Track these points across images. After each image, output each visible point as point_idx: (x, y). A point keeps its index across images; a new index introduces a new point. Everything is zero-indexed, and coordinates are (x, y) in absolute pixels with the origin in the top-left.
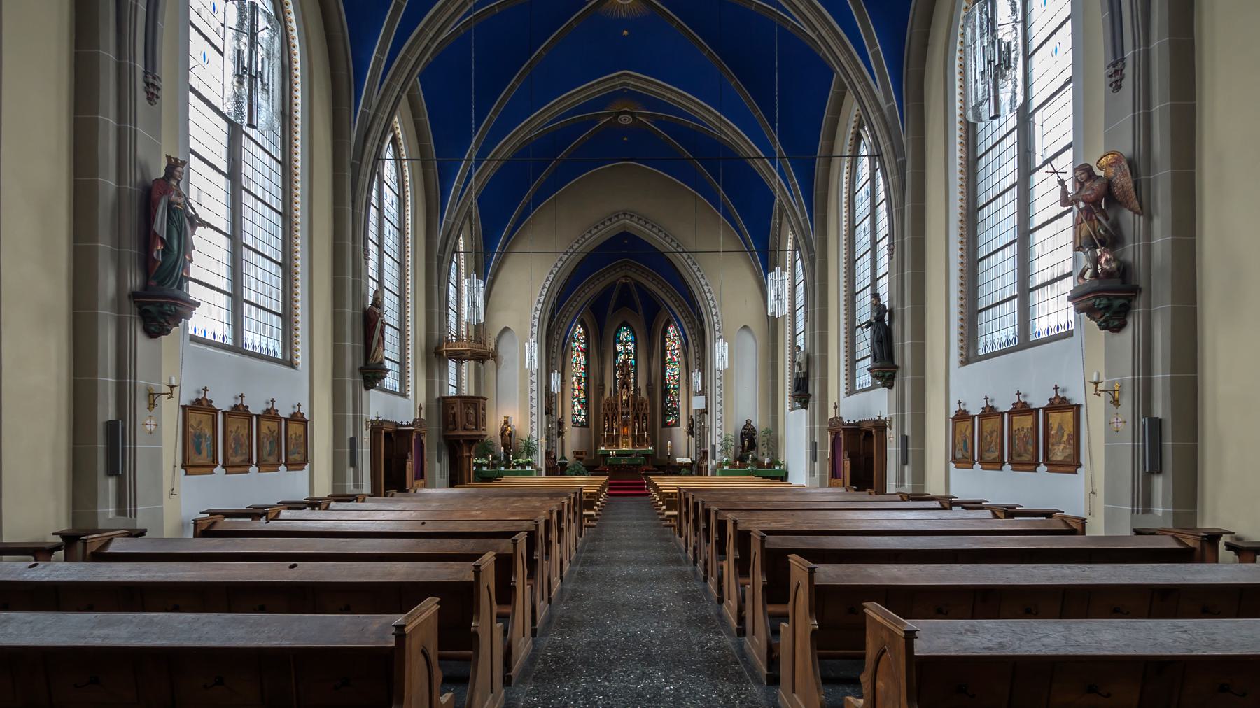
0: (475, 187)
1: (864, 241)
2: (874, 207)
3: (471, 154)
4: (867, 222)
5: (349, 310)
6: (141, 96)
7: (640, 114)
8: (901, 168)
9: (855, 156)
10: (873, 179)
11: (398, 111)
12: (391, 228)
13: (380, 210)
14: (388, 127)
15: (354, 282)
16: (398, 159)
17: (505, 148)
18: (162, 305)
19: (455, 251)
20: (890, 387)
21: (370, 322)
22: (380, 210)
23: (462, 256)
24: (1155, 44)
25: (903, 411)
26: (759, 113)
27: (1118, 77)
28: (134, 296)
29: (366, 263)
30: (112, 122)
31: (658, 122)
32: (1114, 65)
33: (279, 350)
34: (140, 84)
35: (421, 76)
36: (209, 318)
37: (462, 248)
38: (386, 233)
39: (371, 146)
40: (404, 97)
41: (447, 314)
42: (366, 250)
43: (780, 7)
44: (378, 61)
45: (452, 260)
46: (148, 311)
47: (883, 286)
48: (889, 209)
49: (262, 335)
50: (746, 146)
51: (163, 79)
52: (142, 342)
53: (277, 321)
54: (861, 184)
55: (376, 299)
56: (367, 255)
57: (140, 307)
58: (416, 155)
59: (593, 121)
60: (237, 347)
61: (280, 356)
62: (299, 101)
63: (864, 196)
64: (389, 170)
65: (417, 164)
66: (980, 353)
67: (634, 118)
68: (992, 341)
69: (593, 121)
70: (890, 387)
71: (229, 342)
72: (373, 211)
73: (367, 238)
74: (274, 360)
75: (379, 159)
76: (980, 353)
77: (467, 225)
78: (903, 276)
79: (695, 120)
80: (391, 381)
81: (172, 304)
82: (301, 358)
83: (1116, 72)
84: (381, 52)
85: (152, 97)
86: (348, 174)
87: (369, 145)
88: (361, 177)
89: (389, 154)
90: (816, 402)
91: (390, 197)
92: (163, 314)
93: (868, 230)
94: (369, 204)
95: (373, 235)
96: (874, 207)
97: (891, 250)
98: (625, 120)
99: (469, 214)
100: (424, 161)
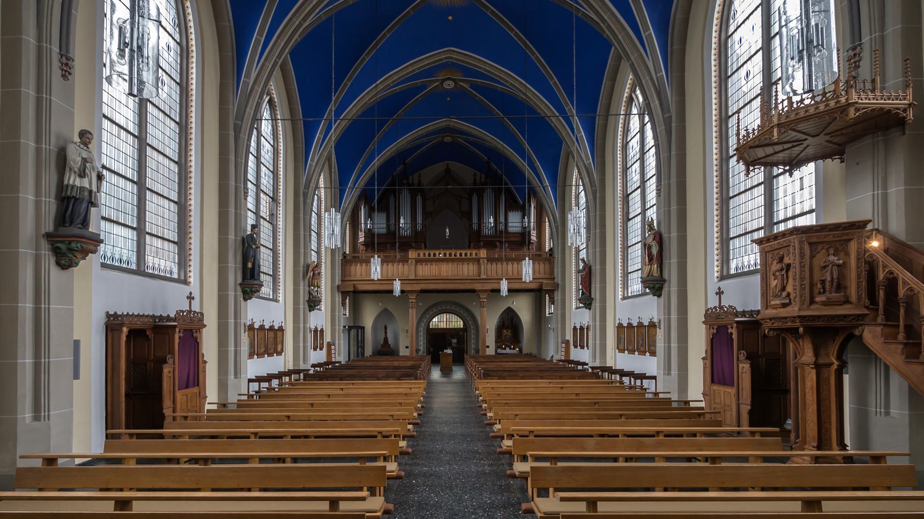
0: (333, 135)
1: (635, 179)
2: (643, 153)
3: (331, 110)
4: (637, 165)
5: (231, 237)
6: (57, 73)
7: (461, 80)
8: (668, 122)
9: (628, 114)
10: (642, 131)
11: (273, 78)
12: (267, 171)
13: (258, 158)
14: (265, 90)
15: (236, 213)
16: (274, 119)
17: (353, 110)
18: (70, 243)
19: (317, 187)
20: (659, 296)
21: (249, 247)
22: (258, 158)
23: (323, 191)
24: (889, 30)
25: (669, 314)
26: (554, 82)
27: (857, 58)
28: (48, 236)
29: (246, 199)
30: (32, 93)
31: (474, 86)
32: (854, 49)
33: (175, 270)
34: (56, 64)
35: (292, 53)
36: (117, 242)
37: (322, 184)
38: (263, 175)
39: (250, 111)
40: (277, 68)
41: (310, 235)
42: (246, 188)
43: (577, 3)
44: (258, 41)
45: (314, 194)
46: (60, 248)
47: (652, 214)
48: (658, 154)
49: (162, 258)
50: (544, 106)
51: (76, 60)
52: (55, 273)
53: (174, 248)
54: (633, 134)
55: (253, 227)
56: (246, 193)
57: (52, 245)
58: (288, 116)
59: (424, 87)
60: (140, 271)
61: (175, 276)
62: (194, 76)
63: (635, 146)
64: (266, 127)
65: (288, 123)
66: (732, 272)
67: (456, 83)
68: (743, 263)
69: (424, 87)
70: (659, 296)
71: (134, 267)
72: (251, 158)
73: (246, 180)
74: (171, 280)
75: (257, 119)
76: (732, 272)
77: (326, 167)
78: (669, 211)
79: (502, 84)
80: (266, 290)
81: (77, 242)
82: (193, 278)
83: (855, 55)
84: (260, 34)
85: (66, 73)
86: (232, 133)
87: (248, 110)
88: (242, 135)
89: (266, 114)
90: (597, 304)
91: (266, 147)
92: (71, 250)
93: (638, 171)
94: (248, 152)
95: (251, 176)
96: (643, 153)
97: (659, 190)
98: (449, 85)
99: (329, 159)
100: (293, 121)
